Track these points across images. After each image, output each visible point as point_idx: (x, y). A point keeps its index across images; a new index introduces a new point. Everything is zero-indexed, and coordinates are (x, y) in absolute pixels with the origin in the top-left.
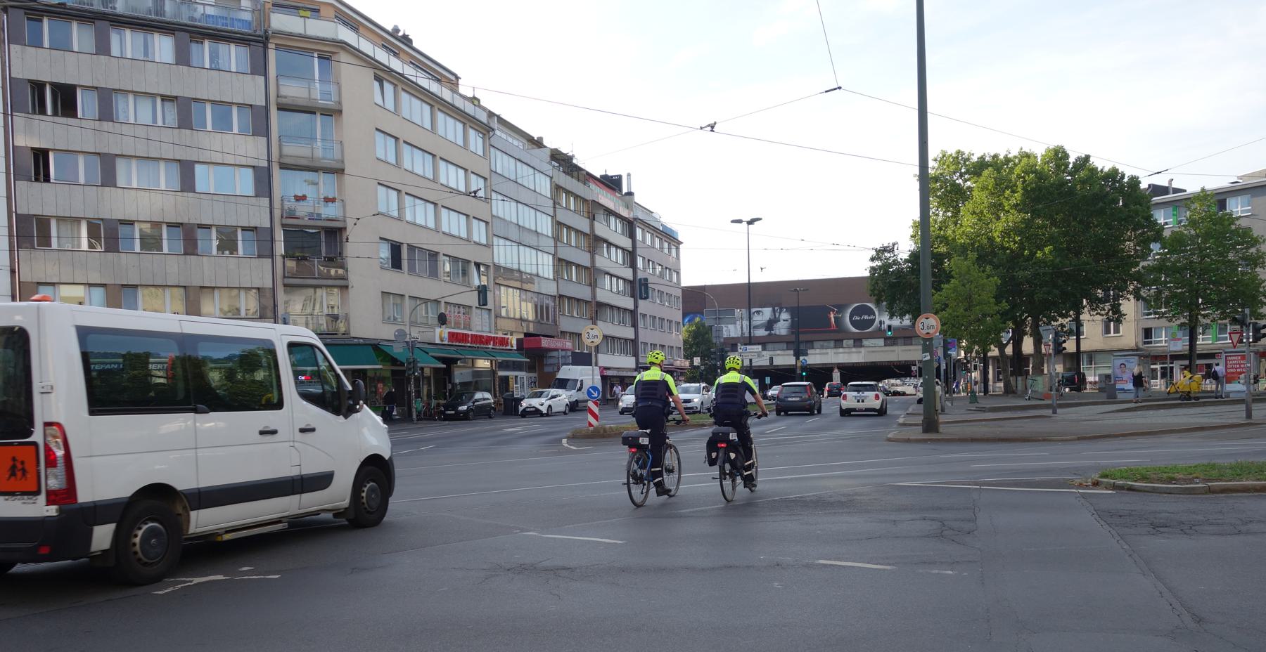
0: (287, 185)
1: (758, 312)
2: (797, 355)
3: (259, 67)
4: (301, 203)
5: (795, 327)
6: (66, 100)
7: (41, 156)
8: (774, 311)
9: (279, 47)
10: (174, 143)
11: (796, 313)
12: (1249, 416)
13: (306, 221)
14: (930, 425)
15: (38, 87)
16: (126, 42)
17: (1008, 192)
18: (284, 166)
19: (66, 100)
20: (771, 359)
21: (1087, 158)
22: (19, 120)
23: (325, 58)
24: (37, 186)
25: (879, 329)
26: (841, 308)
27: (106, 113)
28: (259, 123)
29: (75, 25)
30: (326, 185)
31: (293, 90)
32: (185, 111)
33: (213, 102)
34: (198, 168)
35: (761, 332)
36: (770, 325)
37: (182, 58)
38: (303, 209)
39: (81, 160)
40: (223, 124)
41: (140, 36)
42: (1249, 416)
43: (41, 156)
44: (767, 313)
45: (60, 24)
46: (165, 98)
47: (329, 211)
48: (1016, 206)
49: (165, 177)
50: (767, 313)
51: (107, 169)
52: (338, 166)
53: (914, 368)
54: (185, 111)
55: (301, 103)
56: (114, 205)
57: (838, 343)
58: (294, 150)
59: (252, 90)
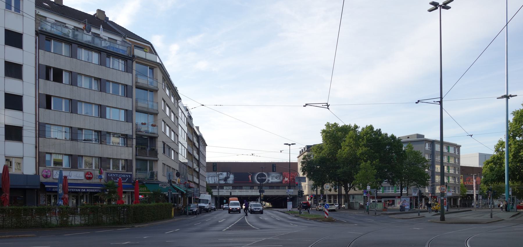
0: (139, 119)
1: (221, 174)
2: (260, 192)
3: (128, 69)
4: (143, 126)
5: (235, 180)
6: (58, 75)
7: (48, 98)
8: (227, 174)
9: (137, 62)
10: (98, 98)
11: (235, 175)
12: (419, 215)
13: (144, 134)
14: (443, 219)
15: (48, 68)
16: (83, 54)
17: (360, 140)
18: (137, 111)
19: (58, 75)
20: (231, 193)
21: (380, 130)
22: (42, 81)
23: (152, 68)
24: (48, 110)
25: (268, 183)
26: (253, 174)
27: (73, 82)
28: (127, 91)
29: (63, 44)
30: (150, 119)
31: (142, 81)
32: (102, 84)
33: (113, 82)
34: (108, 109)
35: (222, 182)
36: (226, 179)
37: (102, 63)
38: (143, 128)
39: (64, 101)
40: (115, 93)
41: (87, 52)
42: (419, 215)
43: (48, 98)
44: (225, 174)
45: (58, 44)
46: (96, 79)
47: (151, 129)
48: (364, 145)
49: (94, 111)
50: (225, 174)
51: (73, 105)
52: (156, 112)
53: (288, 198)
54: (102, 84)
55: (145, 86)
56: (77, 122)
57: (252, 188)
58: (142, 105)
59: (127, 79)
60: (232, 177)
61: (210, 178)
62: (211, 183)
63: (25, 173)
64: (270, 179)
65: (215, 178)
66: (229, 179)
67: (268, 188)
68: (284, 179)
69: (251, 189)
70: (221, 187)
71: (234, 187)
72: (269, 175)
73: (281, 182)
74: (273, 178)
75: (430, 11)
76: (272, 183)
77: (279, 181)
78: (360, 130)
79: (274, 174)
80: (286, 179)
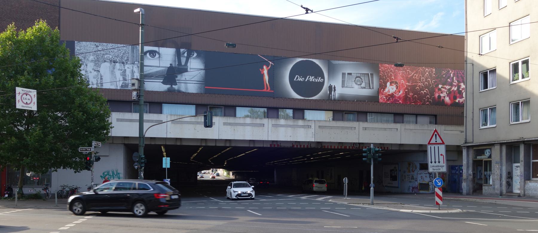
5: (209, 79)
8: (178, 55)
26: (278, 62)
35: (156, 86)
36: (171, 75)
44: (167, 56)
57: (273, 111)
60: (195, 67)
61: (105, 68)
62: (107, 86)
63: (144, 123)
64: (337, 83)
65: (128, 68)
66: (186, 76)
67: (391, 117)
68: (383, 86)
69: (267, 116)
70: (155, 103)
71: (207, 107)
72: (332, 70)
73: (374, 99)
74: (348, 82)
75: (101, 176)
76: (343, 99)
77: (366, 92)
78: (62, 167)
79: (349, 68)
80: (391, 89)
